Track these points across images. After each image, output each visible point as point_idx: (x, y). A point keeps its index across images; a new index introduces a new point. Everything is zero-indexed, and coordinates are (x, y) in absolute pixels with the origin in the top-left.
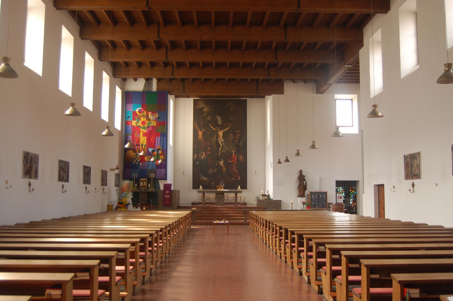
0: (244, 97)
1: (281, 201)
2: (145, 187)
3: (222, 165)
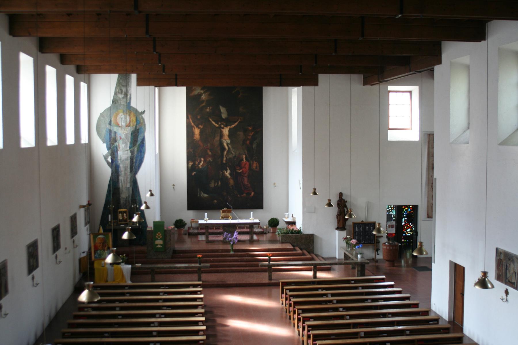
1: (312, 235)
2: (125, 221)
3: (227, 172)
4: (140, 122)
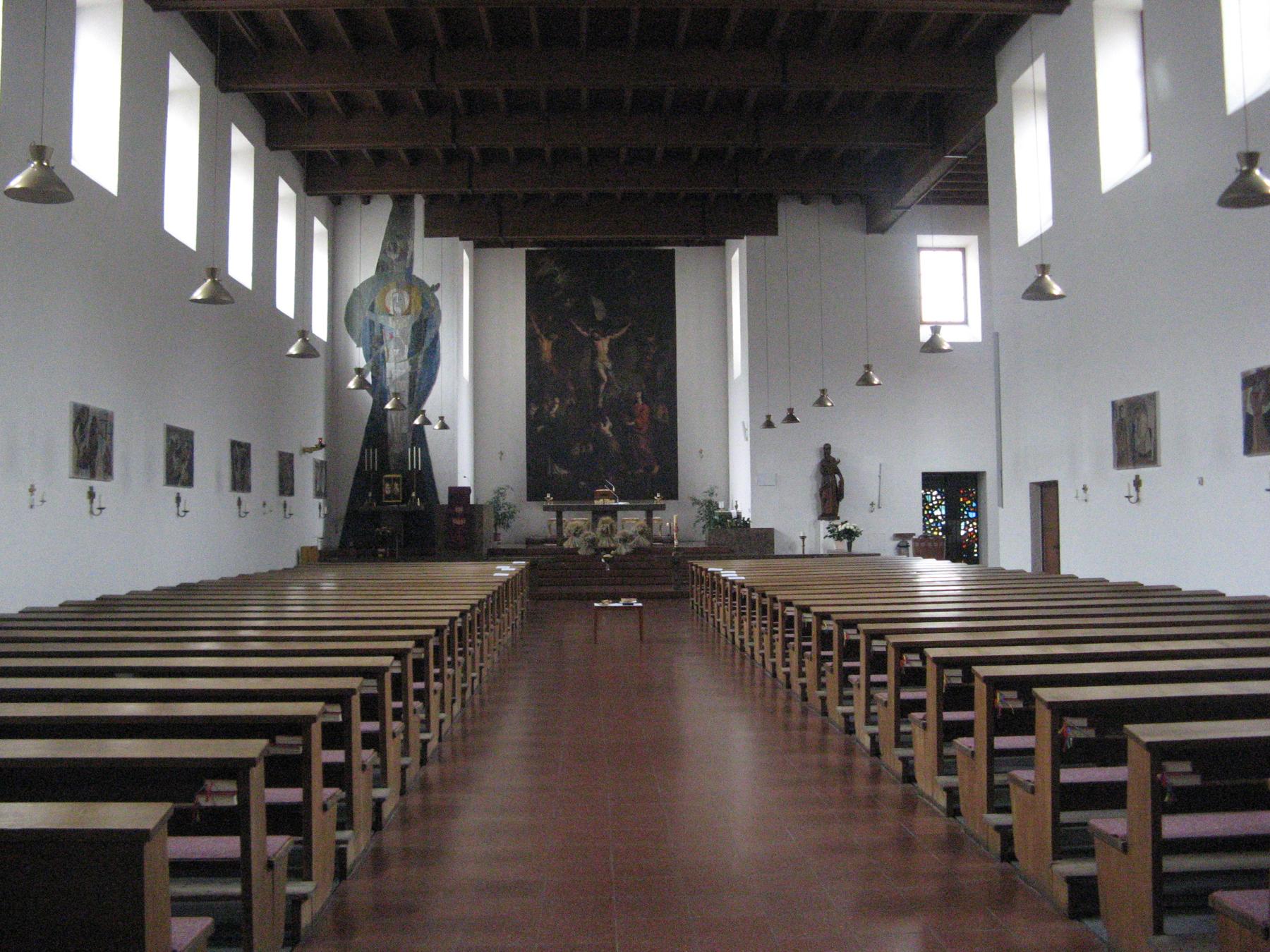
0: (666, 243)
2: (396, 497)
3: (605, 410)
4: (430, 307)
